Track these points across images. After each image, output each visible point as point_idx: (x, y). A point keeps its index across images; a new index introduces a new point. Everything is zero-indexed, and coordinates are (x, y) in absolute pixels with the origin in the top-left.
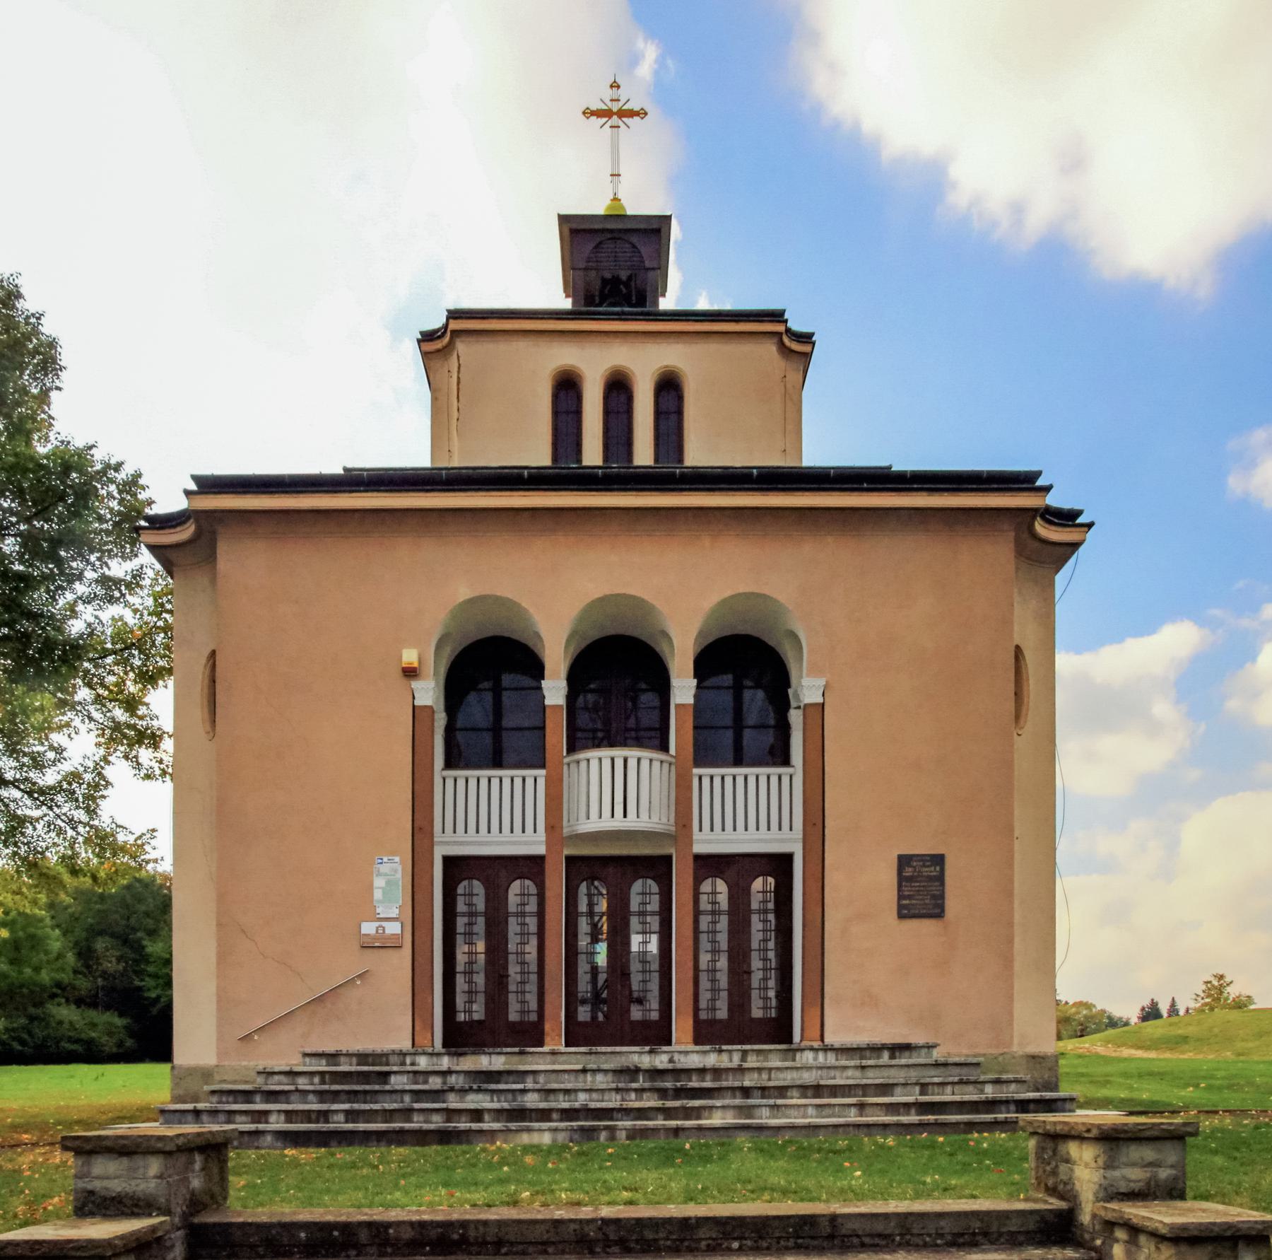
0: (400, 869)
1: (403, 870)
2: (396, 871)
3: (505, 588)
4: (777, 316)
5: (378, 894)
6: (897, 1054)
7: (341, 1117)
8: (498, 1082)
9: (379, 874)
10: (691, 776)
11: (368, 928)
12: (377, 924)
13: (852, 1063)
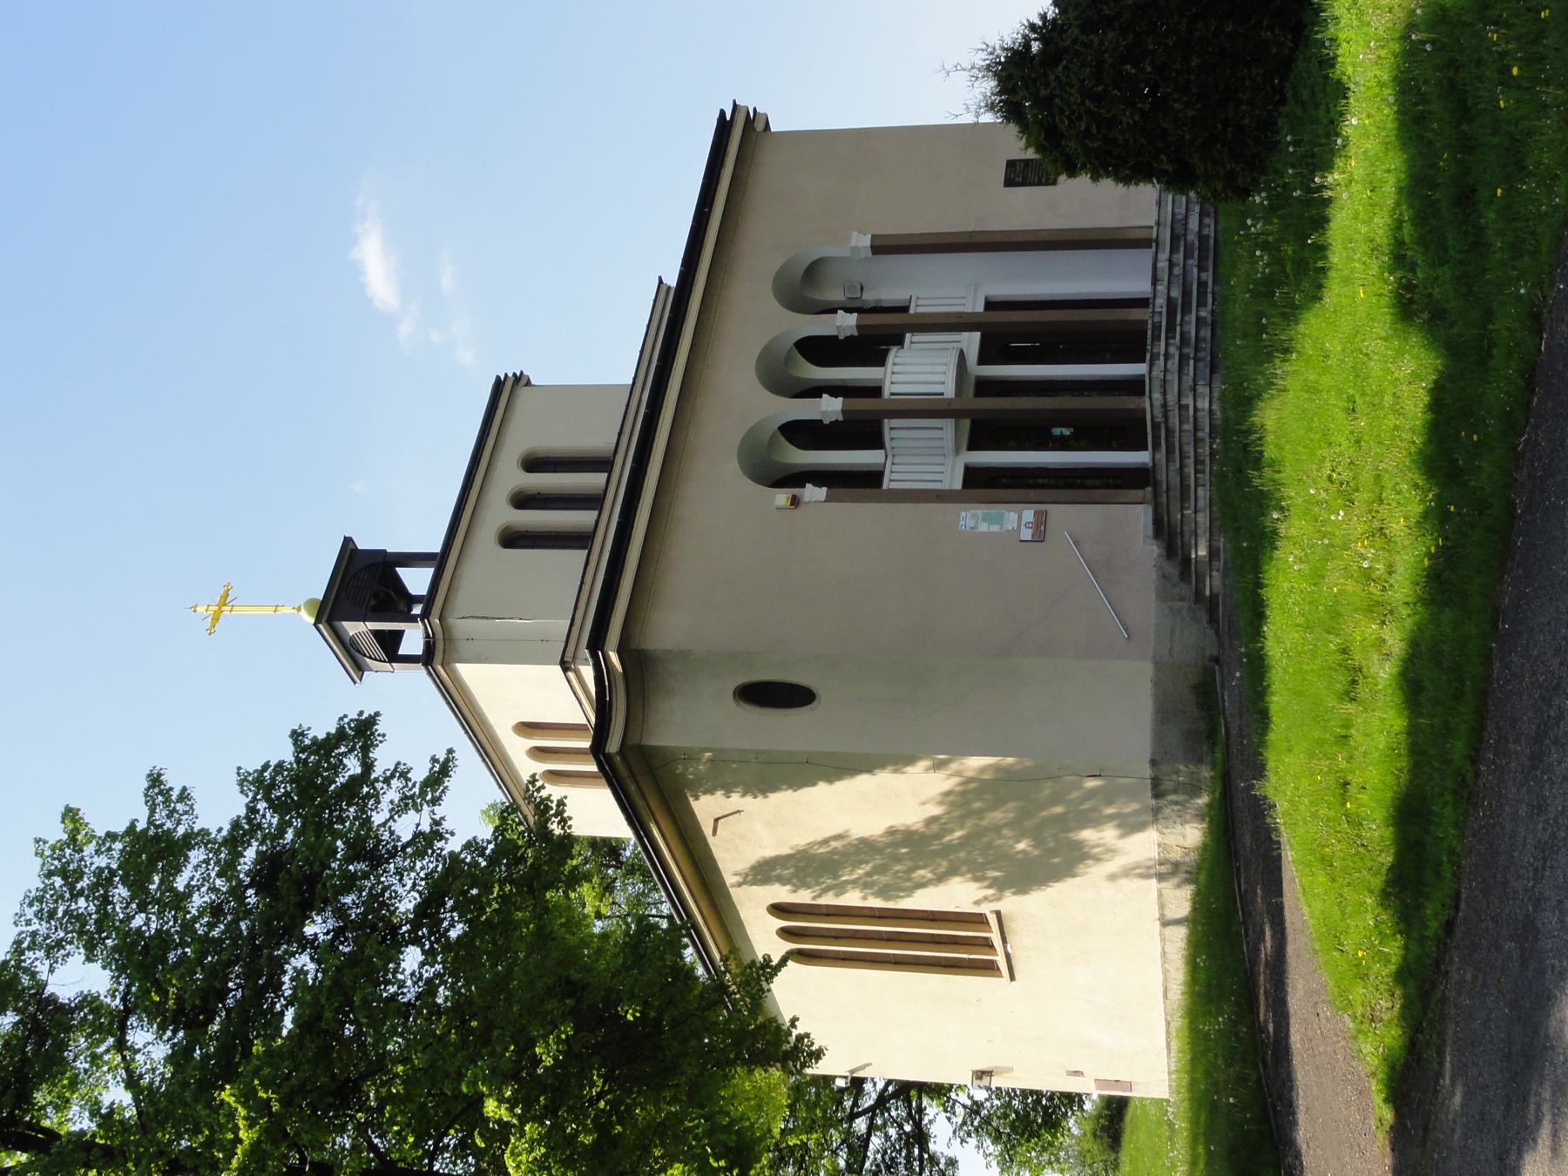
0: (972, 511)
1: (974, 509)
3: (735, 437)
4: (499, 385)
5: (995, 528)
6: (1201, 458)
7: (1204, 275)
8: (1189, 486)
11: (1027, 534)
12: (1023, 527)
13: (1208, 579)
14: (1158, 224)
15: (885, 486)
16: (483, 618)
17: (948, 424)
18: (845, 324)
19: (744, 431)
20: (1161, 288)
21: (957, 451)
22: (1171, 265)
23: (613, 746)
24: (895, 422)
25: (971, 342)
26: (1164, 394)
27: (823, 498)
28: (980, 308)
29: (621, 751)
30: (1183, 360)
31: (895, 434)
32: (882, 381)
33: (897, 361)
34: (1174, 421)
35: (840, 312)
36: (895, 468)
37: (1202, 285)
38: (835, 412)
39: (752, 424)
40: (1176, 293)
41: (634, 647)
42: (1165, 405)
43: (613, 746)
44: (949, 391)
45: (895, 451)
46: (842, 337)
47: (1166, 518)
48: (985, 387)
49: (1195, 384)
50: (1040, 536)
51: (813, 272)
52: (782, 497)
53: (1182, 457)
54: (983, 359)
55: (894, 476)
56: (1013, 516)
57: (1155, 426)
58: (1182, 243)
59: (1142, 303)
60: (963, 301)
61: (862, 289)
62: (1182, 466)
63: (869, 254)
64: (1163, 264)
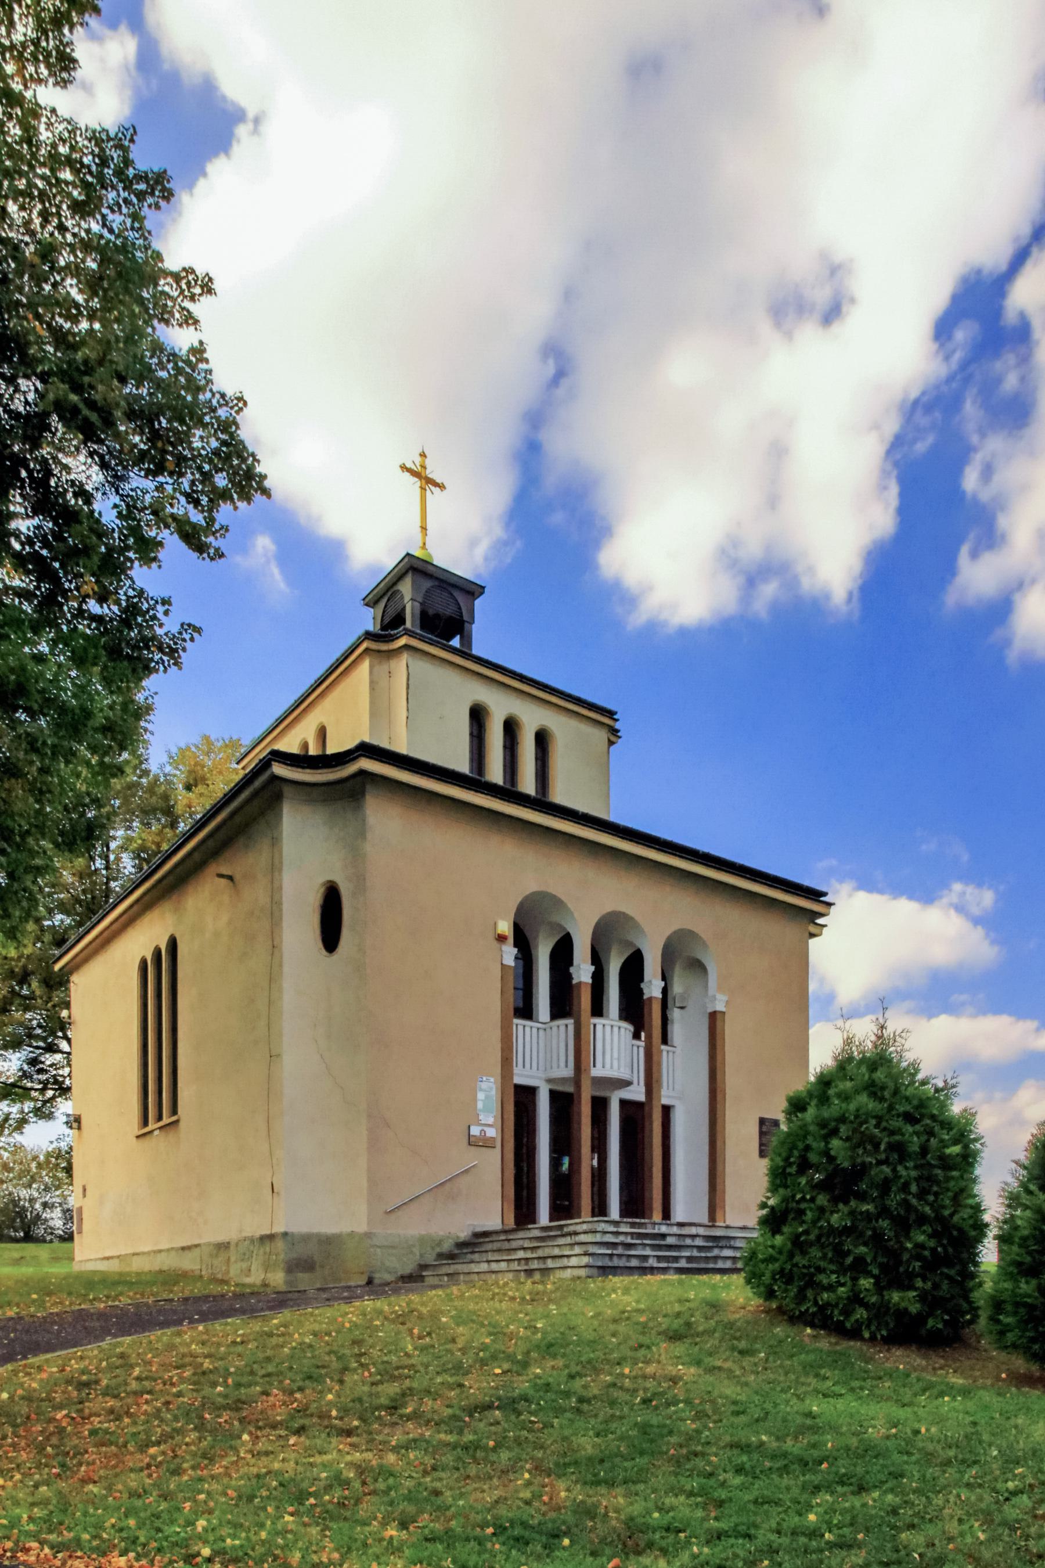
0: (494, 1087)
1: (497, 1089)
2: (491, 1089)
4: (610, 714)
5: (480, 1105)
9: (481, 1090)
10: (512, 1023)
11: (475, 1131)
12: (480, 1128)
14: (727, 1227)
15: (516, 1021)
16: (408, 685)
17: (568, 1072)
18: (653, 987)
19: (563, 898)
20: (675, 1230)
21: (549, 1081)
22: (693, 1237)
23: (279, 769)
24: (571, 1028)
25: (637, 1093)
26: (585, 1233)
27: (505, 962)
28: (665, 1101)
29: (275, 778)
30: (614, 1245)
31: (562, 1029)
32: (608, 1017)
33: (622, 1030)
34: (562, 1241)
35: (663, 984)
36: (535, 1031)
37: (676, 1259)
38: (579, 977)
39: (569, 905)
40: (670, 1240)
41: (368, 787)
42: (576, 1233)
43: (279, 769)
44: (597, 1072)
45: (548, 1030)
46: (643, 985)
47: (487, 1240)
48: (600, 1105)
49: (589, 1255)
50: (472, 1142)
51: (698, 967)
52: (505, 927)
53: (533, 1249)
54: (623, 1103)
55: (528, 1029)
56: (491, 1120)
57: (561, 1227)
58: (711, 1244)
59: (666, 1215)
60: (671, 1087)
61: (682, 1008)
62: (524, 1249)
63: (710, 1010)
64: (693, 1231)
